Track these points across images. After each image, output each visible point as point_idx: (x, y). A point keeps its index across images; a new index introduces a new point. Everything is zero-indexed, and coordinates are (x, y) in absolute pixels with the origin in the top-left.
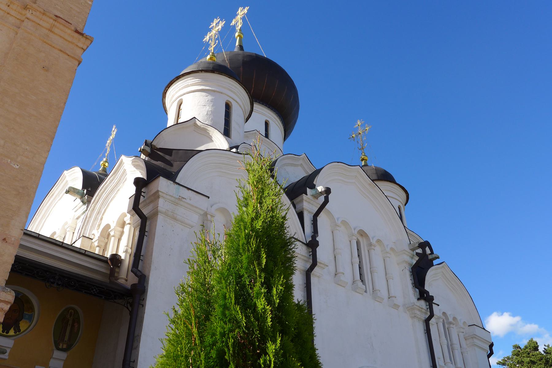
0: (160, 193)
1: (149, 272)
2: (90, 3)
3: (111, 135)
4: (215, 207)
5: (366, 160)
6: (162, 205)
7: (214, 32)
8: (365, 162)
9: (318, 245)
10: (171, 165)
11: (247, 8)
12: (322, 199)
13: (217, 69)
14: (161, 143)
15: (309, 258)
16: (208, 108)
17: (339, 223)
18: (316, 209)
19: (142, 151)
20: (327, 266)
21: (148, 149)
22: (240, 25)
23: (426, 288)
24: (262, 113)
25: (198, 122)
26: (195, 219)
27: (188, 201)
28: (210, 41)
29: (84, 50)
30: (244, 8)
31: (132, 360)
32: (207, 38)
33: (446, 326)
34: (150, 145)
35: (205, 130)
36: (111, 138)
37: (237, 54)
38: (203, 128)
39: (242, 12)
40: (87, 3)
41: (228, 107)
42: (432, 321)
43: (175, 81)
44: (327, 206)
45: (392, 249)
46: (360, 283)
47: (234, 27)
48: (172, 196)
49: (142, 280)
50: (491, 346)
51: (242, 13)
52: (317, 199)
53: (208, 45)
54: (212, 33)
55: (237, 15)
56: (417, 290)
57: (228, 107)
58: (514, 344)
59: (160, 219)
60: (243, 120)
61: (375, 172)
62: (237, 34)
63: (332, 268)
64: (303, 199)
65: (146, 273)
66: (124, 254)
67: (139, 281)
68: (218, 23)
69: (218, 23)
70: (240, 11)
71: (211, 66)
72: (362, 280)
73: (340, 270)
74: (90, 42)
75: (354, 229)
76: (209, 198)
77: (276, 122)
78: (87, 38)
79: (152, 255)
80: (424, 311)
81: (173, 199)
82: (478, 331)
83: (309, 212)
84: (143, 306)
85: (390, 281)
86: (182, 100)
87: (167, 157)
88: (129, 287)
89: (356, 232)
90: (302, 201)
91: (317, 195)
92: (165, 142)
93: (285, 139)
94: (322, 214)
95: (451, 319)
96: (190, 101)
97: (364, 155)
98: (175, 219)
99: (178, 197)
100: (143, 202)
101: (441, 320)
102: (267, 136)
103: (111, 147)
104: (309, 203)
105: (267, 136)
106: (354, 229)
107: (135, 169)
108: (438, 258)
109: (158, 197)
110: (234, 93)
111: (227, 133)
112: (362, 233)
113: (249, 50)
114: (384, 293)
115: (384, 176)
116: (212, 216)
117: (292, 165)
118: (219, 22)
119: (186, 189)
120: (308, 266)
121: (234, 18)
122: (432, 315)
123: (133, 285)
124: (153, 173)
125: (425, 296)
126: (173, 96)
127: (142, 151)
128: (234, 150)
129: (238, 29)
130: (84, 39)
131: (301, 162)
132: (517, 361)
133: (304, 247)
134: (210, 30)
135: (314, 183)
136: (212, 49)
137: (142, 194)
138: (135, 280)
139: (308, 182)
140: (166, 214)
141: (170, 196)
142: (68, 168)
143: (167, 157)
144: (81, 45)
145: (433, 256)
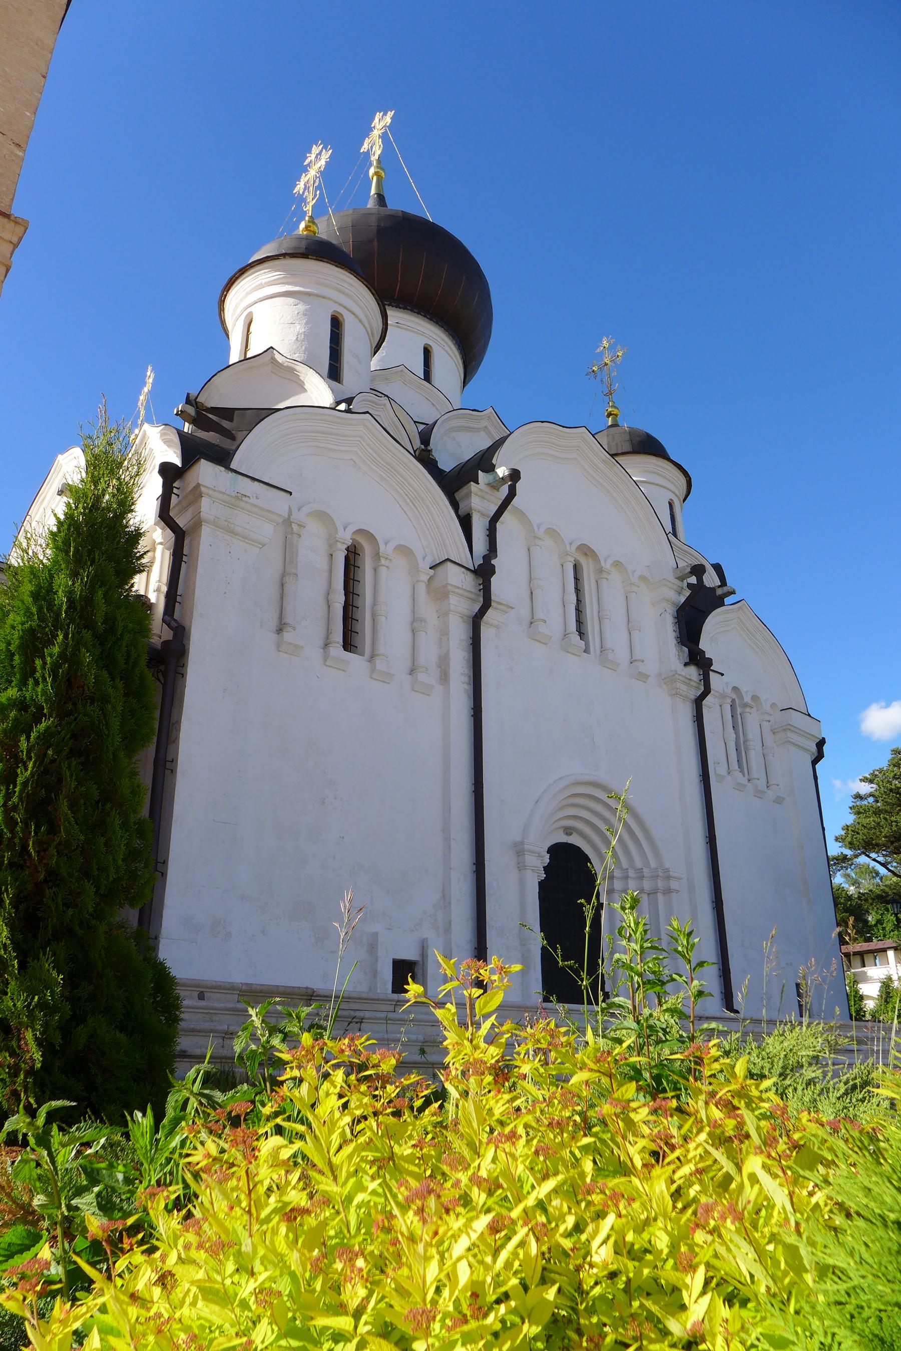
0: (203, 489)
1: (191, 622)
2: (21, 154)
3: (145, 384)
4: (306, 510)
5: (616, 415)
6: (207, 507)
7: (312, 172)
8: (614, 420)
9: (494, 572)
10: (233, 438)
11: (390, 114)
12: (505, 490)
13: (317, 250)
14: (215, 398)
15: (479, 595)
16: (299, 328)
17: (541, 532)
18: (494, 509)
19: (182, 414)
20: (512, 608)
21: (191, 410)
22: (378, 152)
23: (702, 645)
24: (411, 333)
25: (278, 357)
26: (267, 530)
27: (253, 501)
28: (306, 193)
29: (16, 246)
30: (385, 114)
31: (169, 758)
32: (300, 187)
33: (739, 710)
34: (194, 402)
35: (291, 370)
36: (146, 390)
37: (369, 214)
38: (288, 367)
39: (381, 122)
40: (16, 155)
41: (336, 323)
42: (708, 701)
43: (237, 278)
44: (515, 501)
45: (642, 578)
46: (576, 637)
47: (367, 154)
48: (224, 493)
49: (180, 632)
50: (821, 743)
51: (382, 124)
52: (498, 490)
53: (302, 199)
54: (309, 176)
55: (372, 130)
56: (686, 650)
57: (336, 323)
58: (894, 747)
59: (206, 534)
60: (368, 349)
61: (628, 437)
62: (372, 171)
63: (525, 613)
64: (471, 492)
65: (186, 624)
66: (155, 594)
67: (175, 636)
68: (320, 153)
69: (320, 153)
70: (377, 120)
71: (303, 244)
72: (581, 632)
73: (539, 615)
74: (23, 229)
75: (570, 544)
76: (291, 493)
77: (446, 348)
78: (16, 223)
79: (194, 593)
80: (694, 684)
81: (225, 498)
82: (798, 720)
83: (483, 515)
84: (183, 675)
85: (635, 634)
86: (251, 314)
87: (226, 424)
88: (159, 647)
89: (573, 548)
90: (469, 495)
91: (496, 485)
92: (220, 396)
93: (465, 383)
94: (506, 515)
95: (747, 699)
96: (267, 315)
97: (612, 406)
98: (233, 532)
99: (234, 494)
100: (177, 504)
101: (729, 701)
102: (427, 377)
103: (147, 408)
104: (481, 498)
105: (427, 377)
106: (570, 544)
107: (165, 447)
108: (733, 593)
109: (200, 496)
110: (347, 295)
111: (334, 373)
112: (586, 550)
113: (395, 205)
114: (621, 653)
115: (647, 446)
116: (301, 526)
117: (468, 429)
118: (322, 151)
119: (248, 480)
120: (477, 607)
121: (367, 136)
122: (707, 691)
123: (165, 643)
124: (192, 451)
125: (698, 660)
126: (236, 307)
127: (182, 414)
128: (342, 407)
129: (374, 159)
130: (12, 224)
131: (484, 423)
132: (892, 774)
133: (470, 577)
134: (305, 170)
135: (494, 461)
136: (308, 209)
137: (175, 490)
138: (168, 635)
139: (484, 461)
140: (215, 524)
141: (221, 492)
142: (63, 450)
143: (226, 424)
144: (7, 236)
145: (725, 589)
